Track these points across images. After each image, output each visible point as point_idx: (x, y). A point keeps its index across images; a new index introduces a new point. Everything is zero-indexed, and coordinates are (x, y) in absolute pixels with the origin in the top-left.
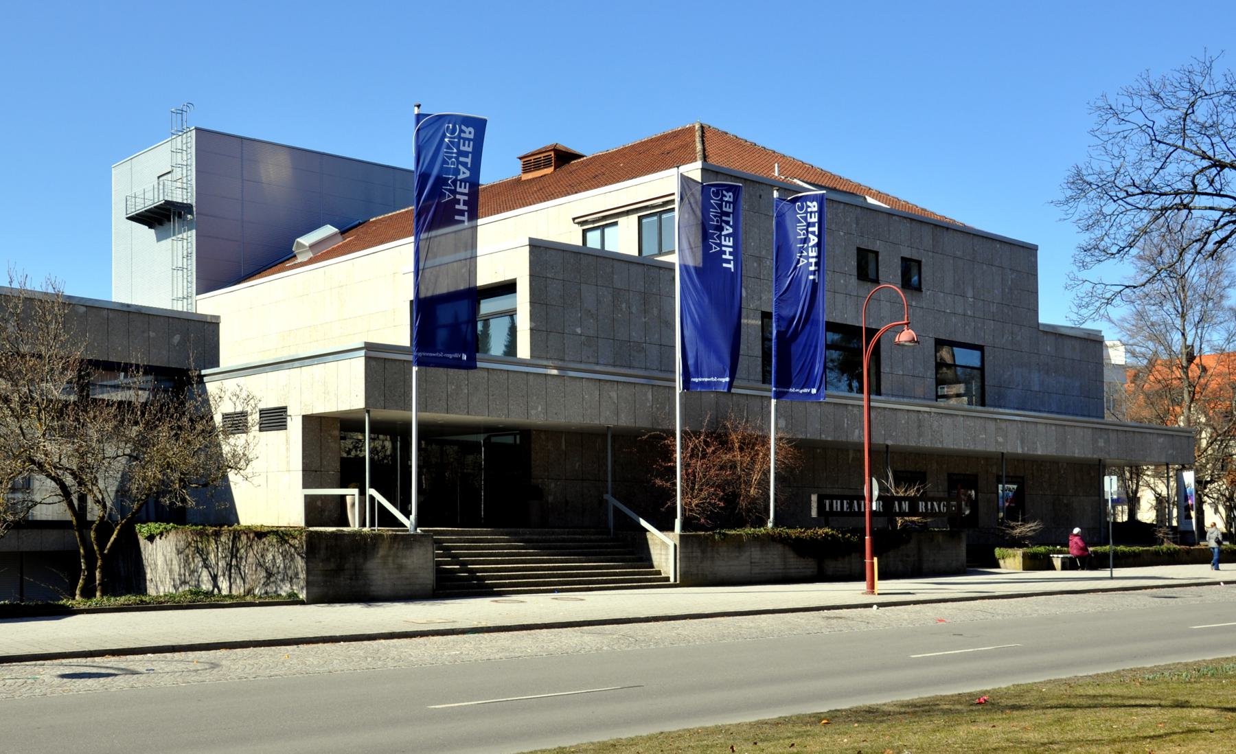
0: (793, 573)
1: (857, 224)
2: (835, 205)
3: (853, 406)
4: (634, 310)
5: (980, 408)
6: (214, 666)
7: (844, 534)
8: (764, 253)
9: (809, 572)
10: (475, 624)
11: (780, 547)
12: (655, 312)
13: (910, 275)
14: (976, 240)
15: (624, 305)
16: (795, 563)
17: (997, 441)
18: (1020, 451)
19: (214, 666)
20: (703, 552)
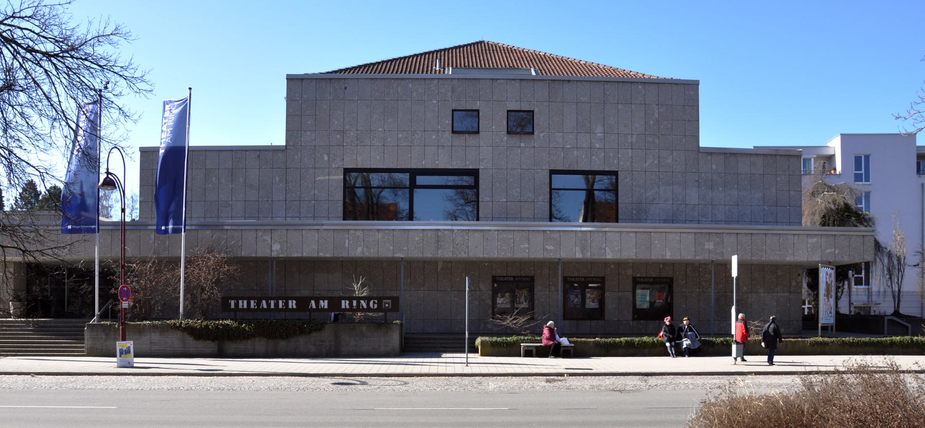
0: (192, 350)
1: (453, 93)
2: (427, 82)
3: (356, 230)
4: (223, 181)
5: (476, 222)
6: (406, 383)
7: (240, 324)
8: (347, 127)
9: (208, 351)
10: (19, 371)
11: (179, 333)
12: (241, 180)
13: (521, 123)
14: (607, 86)
15: (214, 179)
16: (192, 344)
17: (545, 249)
18: (579, 256)
19: (406, 383)
20: (107, 335)
